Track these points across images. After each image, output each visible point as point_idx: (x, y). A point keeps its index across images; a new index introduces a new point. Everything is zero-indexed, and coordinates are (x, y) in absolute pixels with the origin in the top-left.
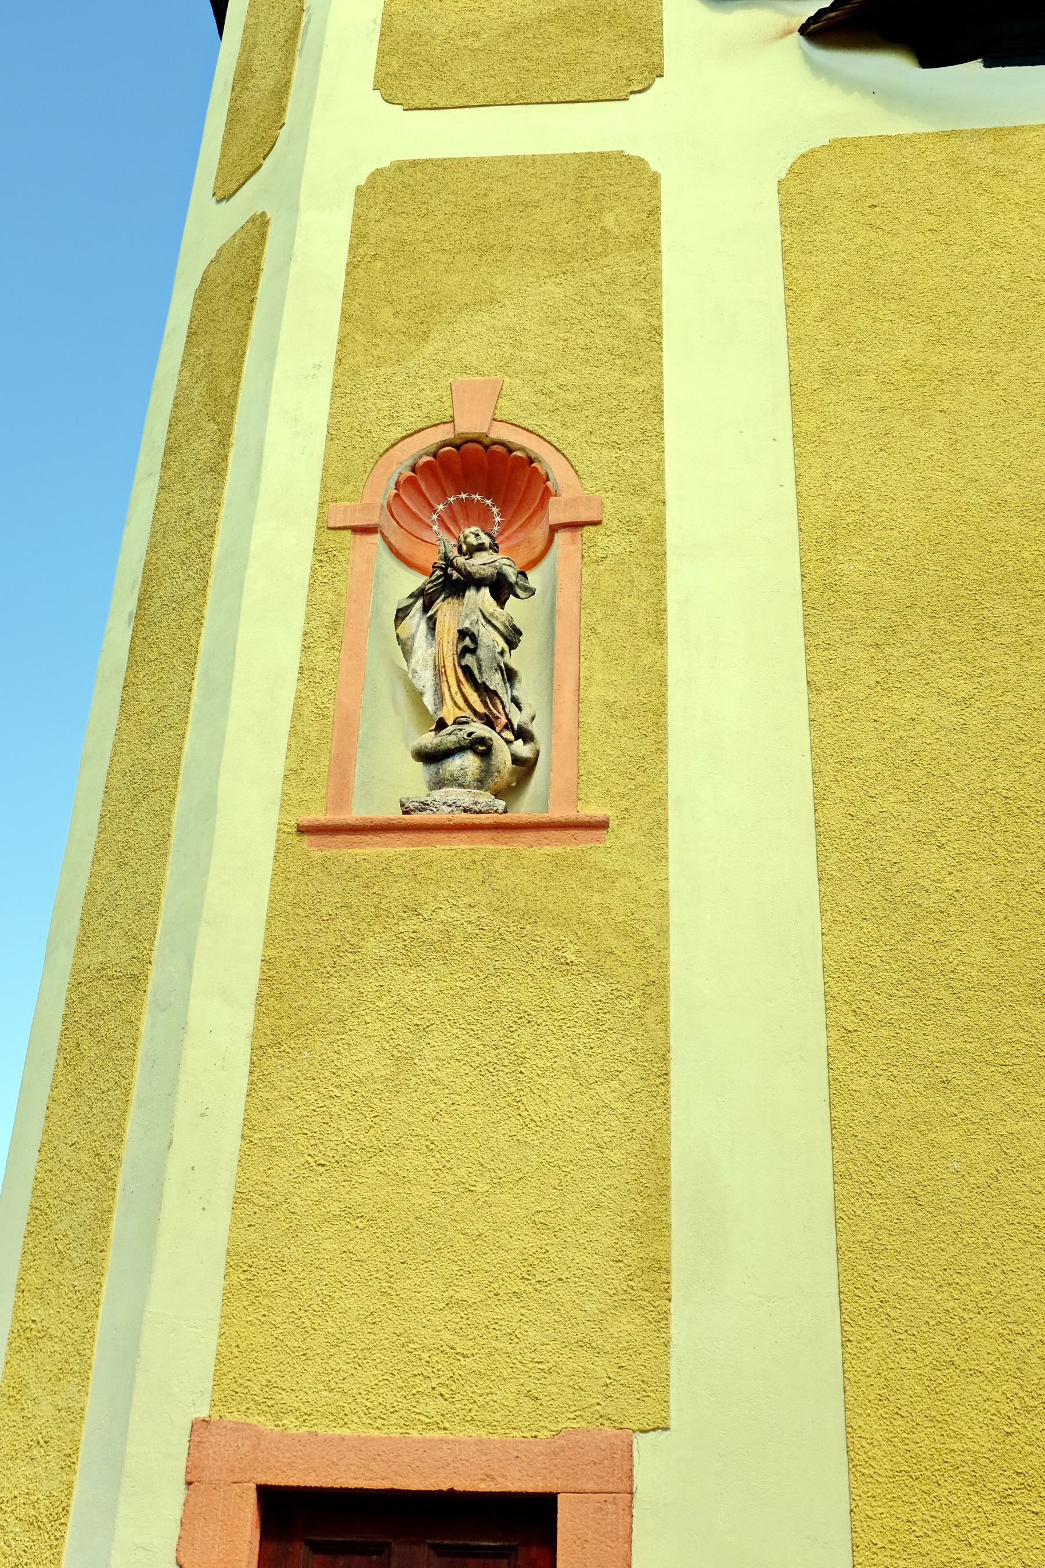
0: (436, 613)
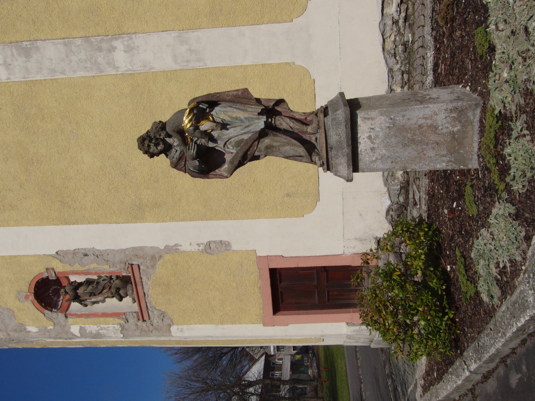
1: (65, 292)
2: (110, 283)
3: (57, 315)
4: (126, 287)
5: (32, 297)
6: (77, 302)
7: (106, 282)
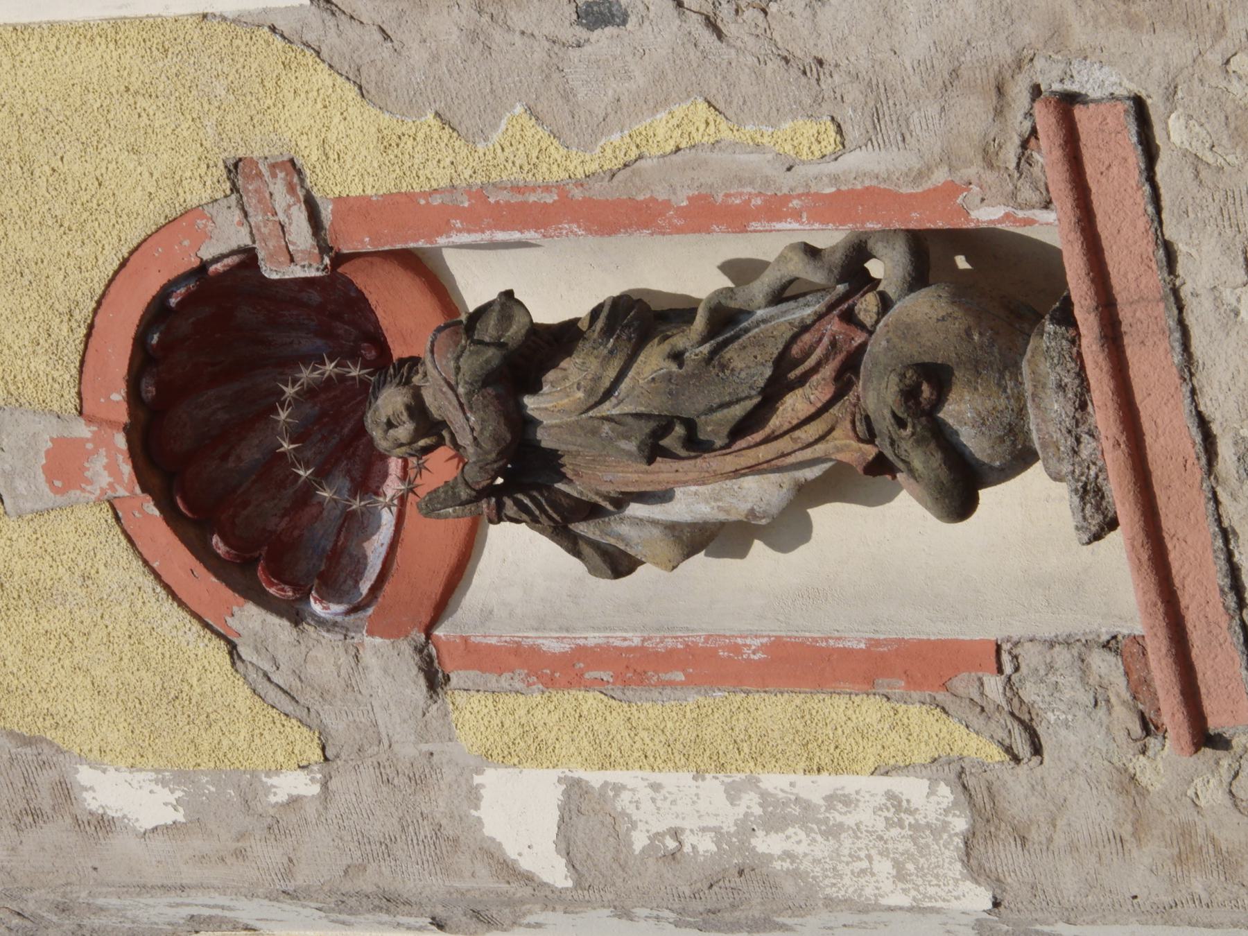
0: (607, 497)
1: (417, 409)
2: (849, 317)
3: (345, 660)
4: (1010, 365)
5: (112, 468)
6: (534, 522)
7: (804, 311)
